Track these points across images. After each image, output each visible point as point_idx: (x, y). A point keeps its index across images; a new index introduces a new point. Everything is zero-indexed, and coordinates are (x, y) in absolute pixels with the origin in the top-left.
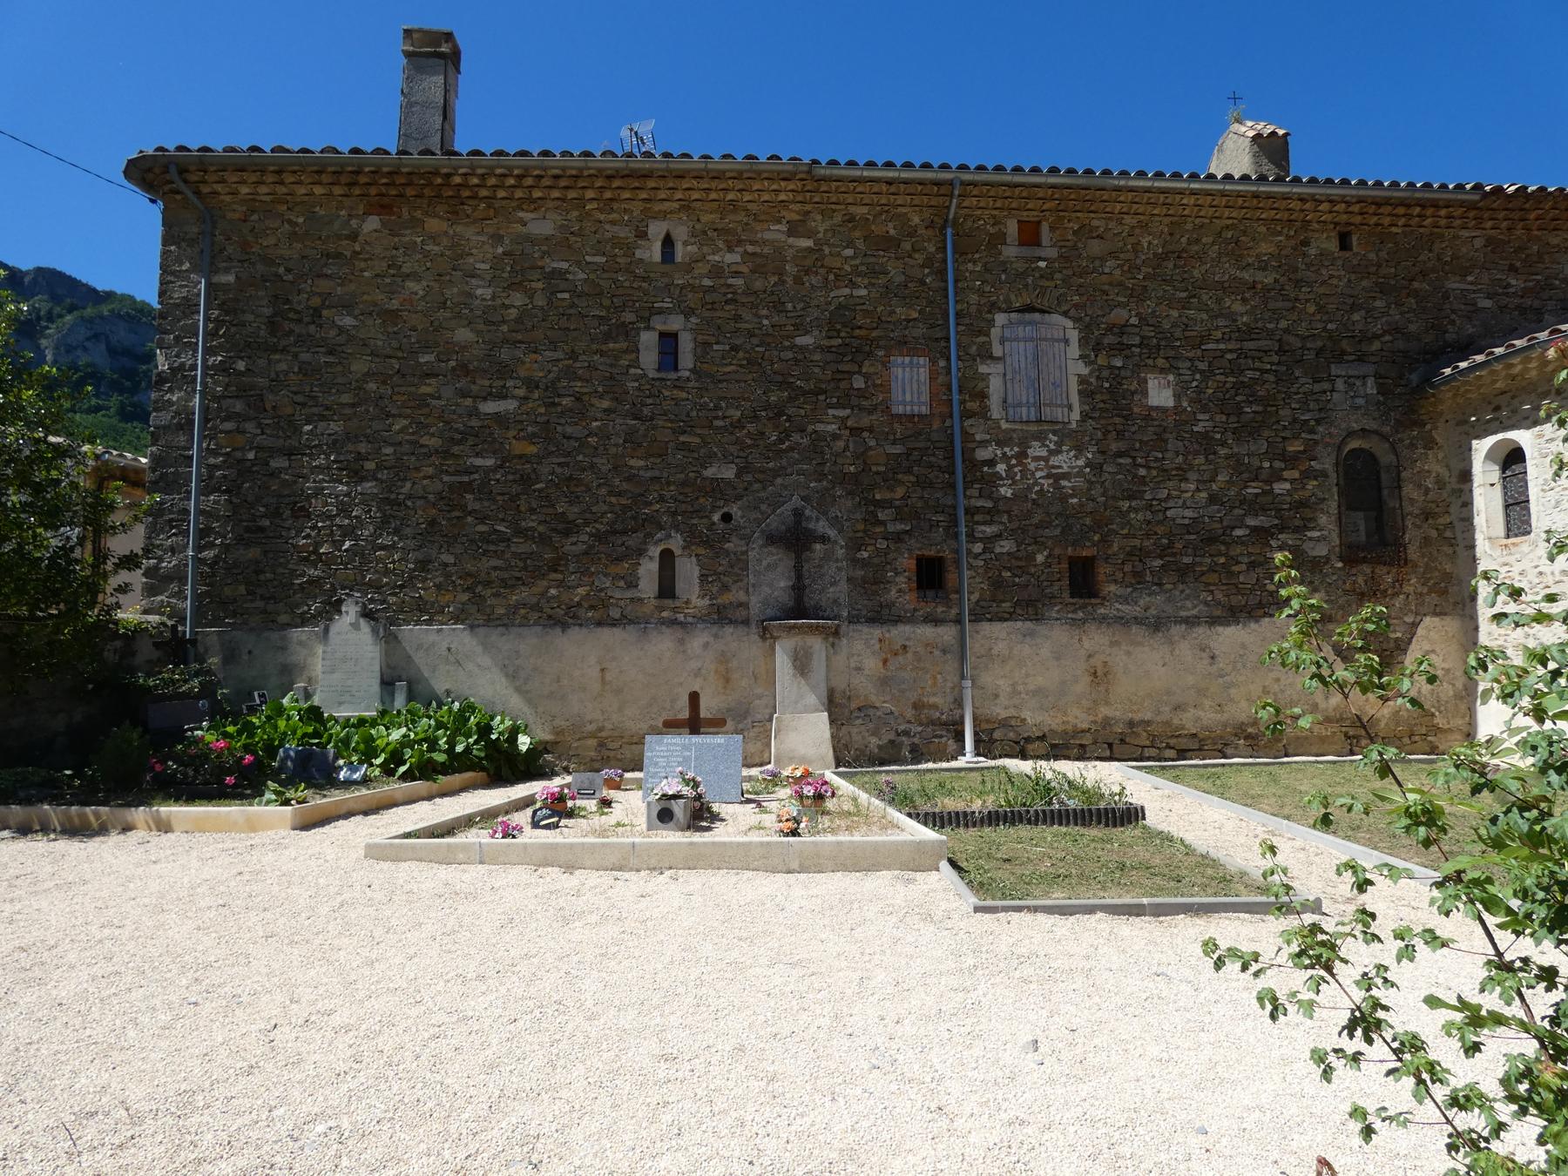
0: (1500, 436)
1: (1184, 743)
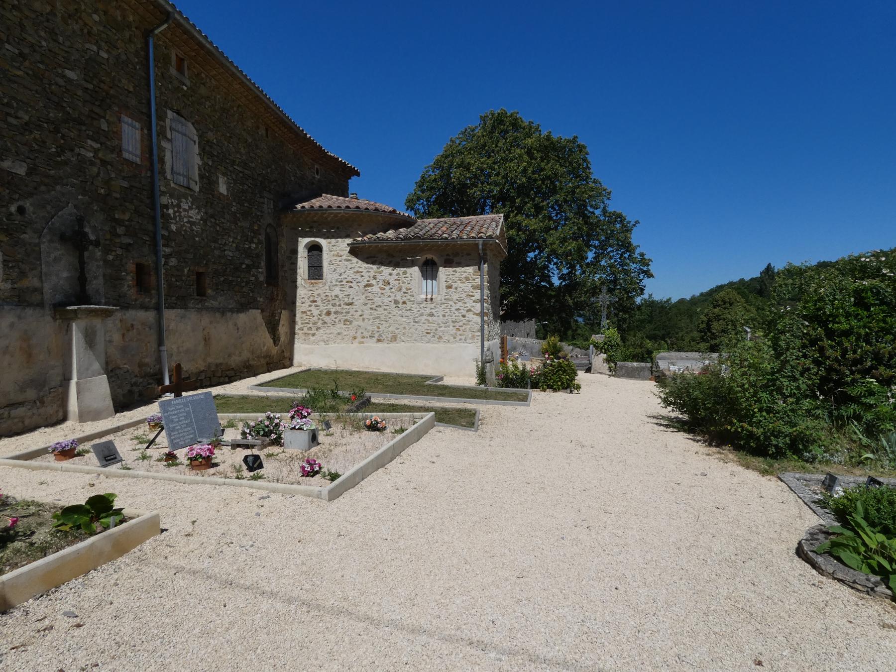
0: (312, 239)
1: (231, 373)
